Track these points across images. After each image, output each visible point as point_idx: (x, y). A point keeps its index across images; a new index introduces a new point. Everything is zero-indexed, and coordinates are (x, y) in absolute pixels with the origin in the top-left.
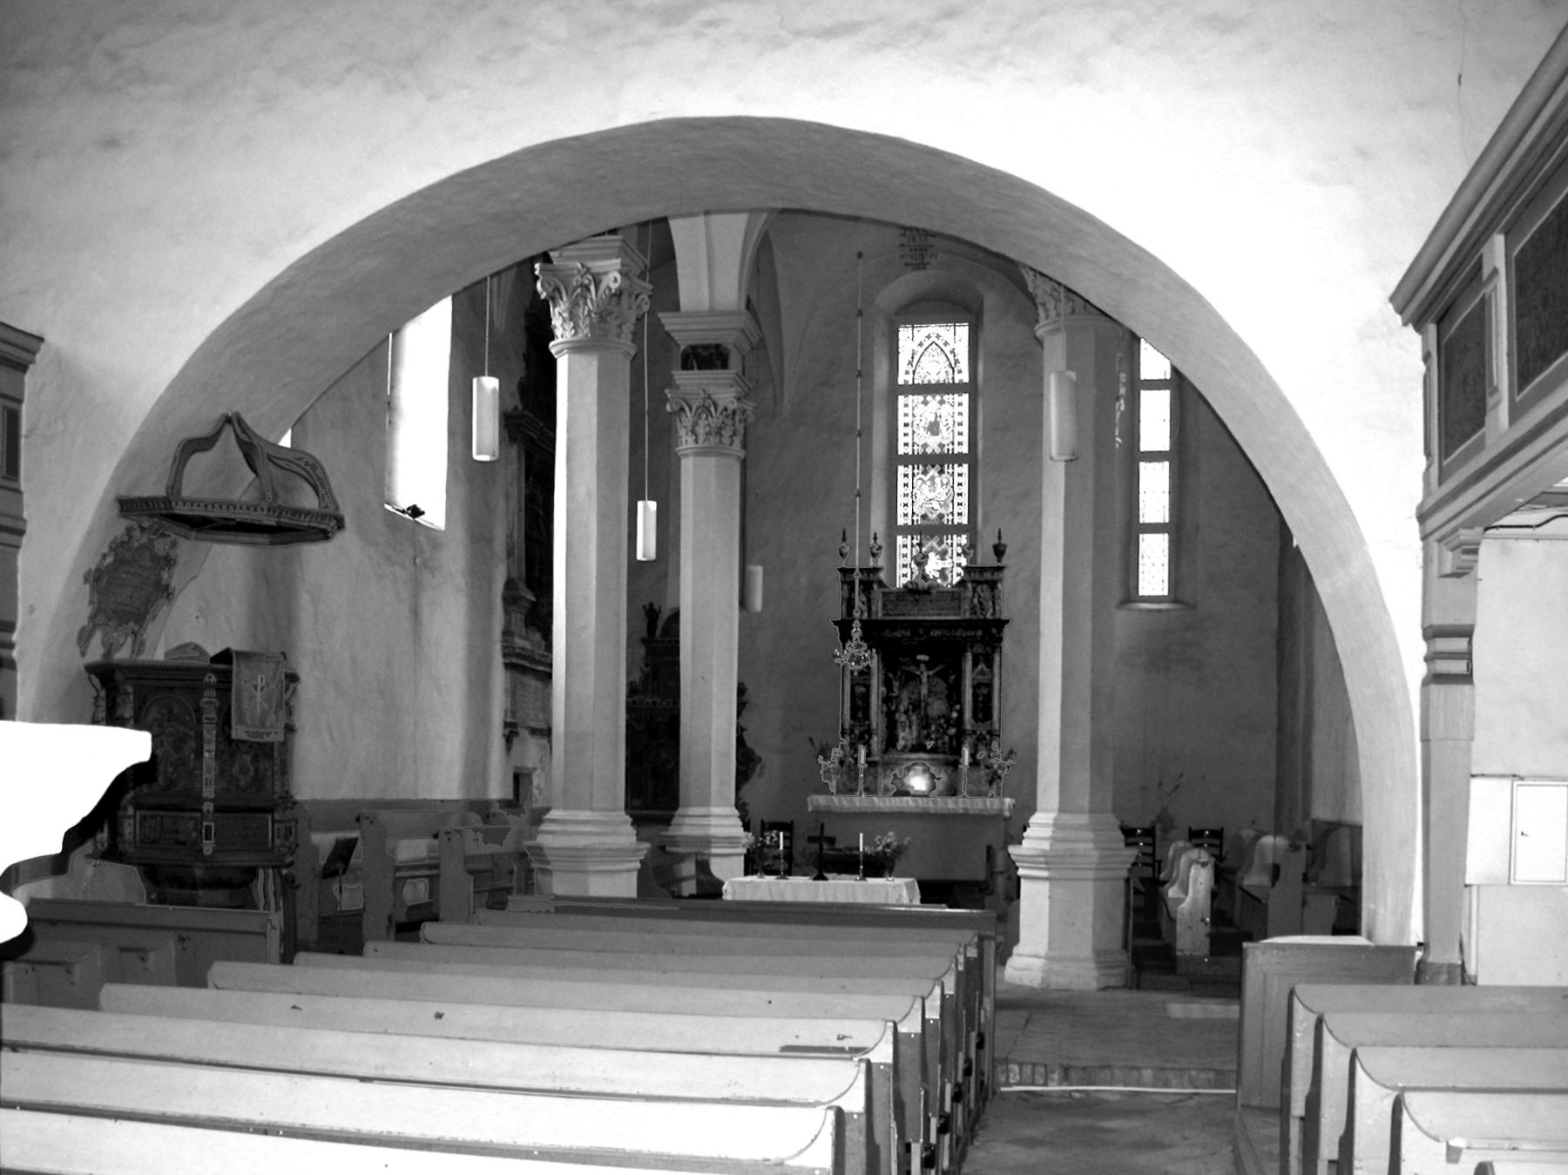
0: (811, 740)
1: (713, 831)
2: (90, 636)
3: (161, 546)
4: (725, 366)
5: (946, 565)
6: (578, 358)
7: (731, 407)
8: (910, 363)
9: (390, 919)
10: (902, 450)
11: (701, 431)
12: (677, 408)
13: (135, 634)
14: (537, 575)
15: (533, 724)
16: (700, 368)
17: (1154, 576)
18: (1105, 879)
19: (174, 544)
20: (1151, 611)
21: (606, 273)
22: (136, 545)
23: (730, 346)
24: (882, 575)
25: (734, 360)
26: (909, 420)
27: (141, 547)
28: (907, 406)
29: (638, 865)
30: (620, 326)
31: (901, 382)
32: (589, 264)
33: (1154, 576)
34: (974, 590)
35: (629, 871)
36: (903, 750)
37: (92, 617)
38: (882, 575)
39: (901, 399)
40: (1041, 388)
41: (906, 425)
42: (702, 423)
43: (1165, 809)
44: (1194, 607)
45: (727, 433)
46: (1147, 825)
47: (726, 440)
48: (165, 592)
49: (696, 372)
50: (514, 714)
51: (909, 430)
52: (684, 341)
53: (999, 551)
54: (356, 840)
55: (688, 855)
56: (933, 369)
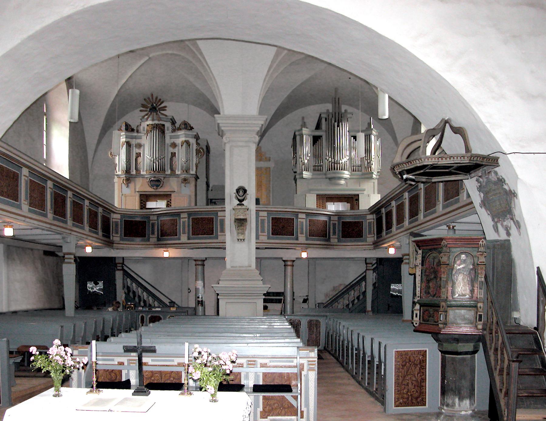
2: (497, 228)
3: (493, 177)
13: (512, 219)
18: (105, 241)
19: (496, 173)
22: (484, 184)
27: (486, 183)
37: (493, 220)
40: (318, 399)
48: (512, 194)
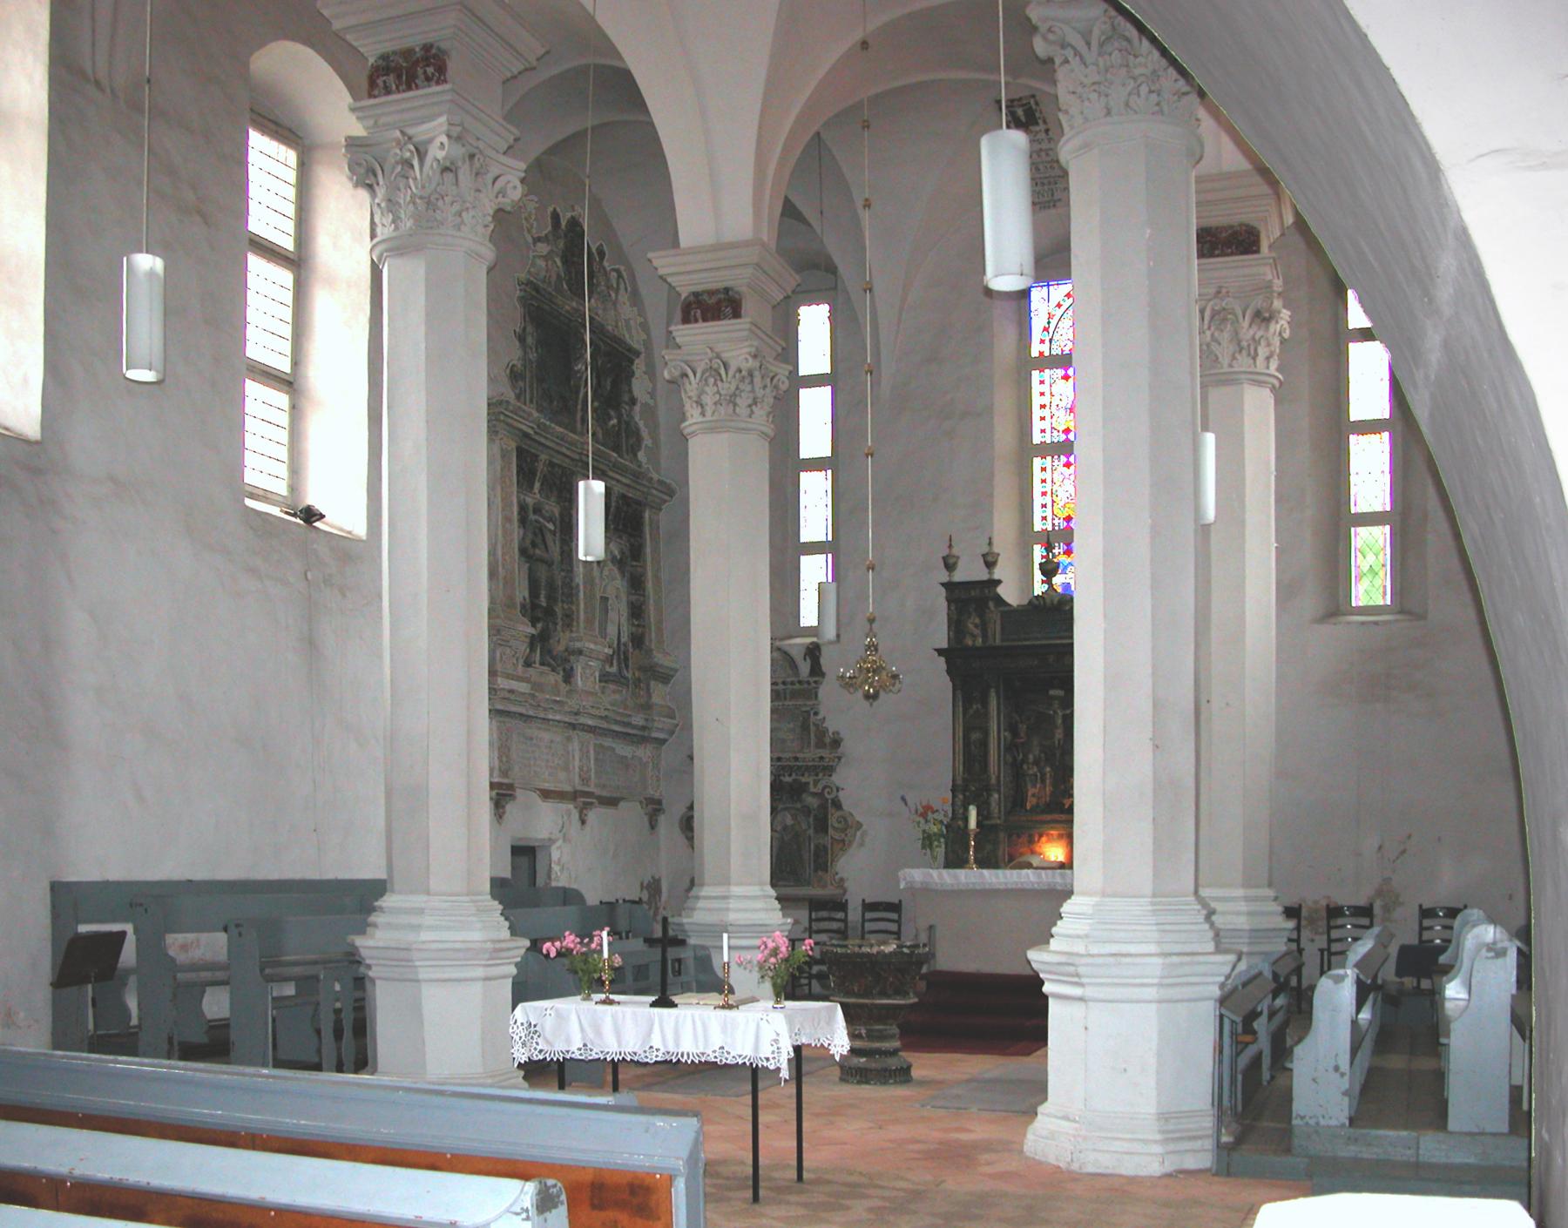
0: (903, 799)
1: (732, 917)
4: (737, 314)
6: (399, 262)
7: (745, 366)
8: (1046, 329)
9: (170, 1040)
10: (1037, 438)
11: (708, 400)
12: (677, 373)
14: (543, 602)
15: (546, 786)
16: (705, 320)
17: (1371, 583)
20: (1363, 623)
21: (431, 141)
23: (744, 289)
25: (748, 306)
26: (1046, 400)
29: (514, 971)
30: (459, 214)
31: (1035, 354)
32: (410, 131)
33: (1371, 583)
35: (504, 977)
36: (1034, 810)
39: (1035, 374)
41: (1043, 406)
42: (710, 390)
43: (1387, 880)
44: (1422, 617)
45: (743, 401)
46: (1361, 901)
47: (742, 410)
49: (701, 324)
50: (504, 773)
51: (1046, 413)
52: (686, 286)
54: (123, 934)
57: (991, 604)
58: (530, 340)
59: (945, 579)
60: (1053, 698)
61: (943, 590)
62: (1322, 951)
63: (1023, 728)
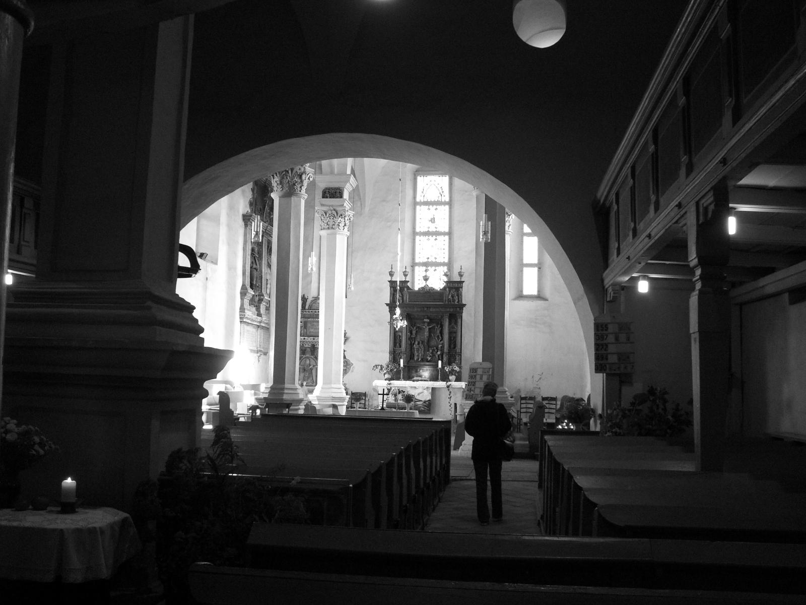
5: (437, 282)
16: (330, 198)
24: (409, 284)
28: (421, 211)
34: (450, 291)
38: (409, 284)
49: (319, 319)
53: (461, 275)
55: (327, 174)
56: (433, 196)
57: (406, 289)
58: (255, 192)
59: (390, 280)
60: (424, 322)
61: (389, 283)
62: (518, 411)
63: (414, 332)
